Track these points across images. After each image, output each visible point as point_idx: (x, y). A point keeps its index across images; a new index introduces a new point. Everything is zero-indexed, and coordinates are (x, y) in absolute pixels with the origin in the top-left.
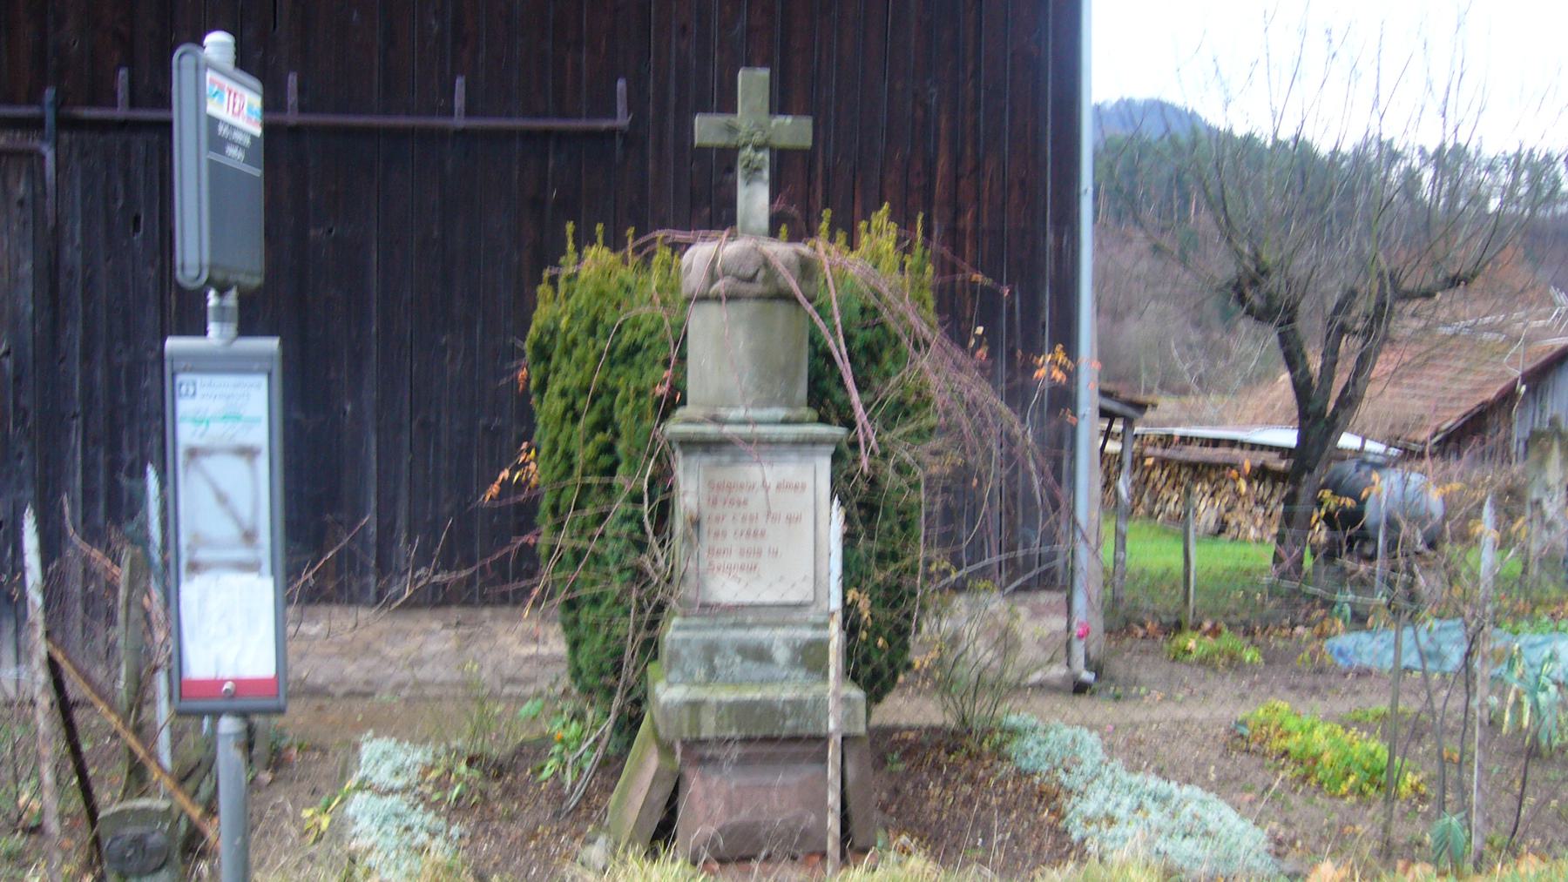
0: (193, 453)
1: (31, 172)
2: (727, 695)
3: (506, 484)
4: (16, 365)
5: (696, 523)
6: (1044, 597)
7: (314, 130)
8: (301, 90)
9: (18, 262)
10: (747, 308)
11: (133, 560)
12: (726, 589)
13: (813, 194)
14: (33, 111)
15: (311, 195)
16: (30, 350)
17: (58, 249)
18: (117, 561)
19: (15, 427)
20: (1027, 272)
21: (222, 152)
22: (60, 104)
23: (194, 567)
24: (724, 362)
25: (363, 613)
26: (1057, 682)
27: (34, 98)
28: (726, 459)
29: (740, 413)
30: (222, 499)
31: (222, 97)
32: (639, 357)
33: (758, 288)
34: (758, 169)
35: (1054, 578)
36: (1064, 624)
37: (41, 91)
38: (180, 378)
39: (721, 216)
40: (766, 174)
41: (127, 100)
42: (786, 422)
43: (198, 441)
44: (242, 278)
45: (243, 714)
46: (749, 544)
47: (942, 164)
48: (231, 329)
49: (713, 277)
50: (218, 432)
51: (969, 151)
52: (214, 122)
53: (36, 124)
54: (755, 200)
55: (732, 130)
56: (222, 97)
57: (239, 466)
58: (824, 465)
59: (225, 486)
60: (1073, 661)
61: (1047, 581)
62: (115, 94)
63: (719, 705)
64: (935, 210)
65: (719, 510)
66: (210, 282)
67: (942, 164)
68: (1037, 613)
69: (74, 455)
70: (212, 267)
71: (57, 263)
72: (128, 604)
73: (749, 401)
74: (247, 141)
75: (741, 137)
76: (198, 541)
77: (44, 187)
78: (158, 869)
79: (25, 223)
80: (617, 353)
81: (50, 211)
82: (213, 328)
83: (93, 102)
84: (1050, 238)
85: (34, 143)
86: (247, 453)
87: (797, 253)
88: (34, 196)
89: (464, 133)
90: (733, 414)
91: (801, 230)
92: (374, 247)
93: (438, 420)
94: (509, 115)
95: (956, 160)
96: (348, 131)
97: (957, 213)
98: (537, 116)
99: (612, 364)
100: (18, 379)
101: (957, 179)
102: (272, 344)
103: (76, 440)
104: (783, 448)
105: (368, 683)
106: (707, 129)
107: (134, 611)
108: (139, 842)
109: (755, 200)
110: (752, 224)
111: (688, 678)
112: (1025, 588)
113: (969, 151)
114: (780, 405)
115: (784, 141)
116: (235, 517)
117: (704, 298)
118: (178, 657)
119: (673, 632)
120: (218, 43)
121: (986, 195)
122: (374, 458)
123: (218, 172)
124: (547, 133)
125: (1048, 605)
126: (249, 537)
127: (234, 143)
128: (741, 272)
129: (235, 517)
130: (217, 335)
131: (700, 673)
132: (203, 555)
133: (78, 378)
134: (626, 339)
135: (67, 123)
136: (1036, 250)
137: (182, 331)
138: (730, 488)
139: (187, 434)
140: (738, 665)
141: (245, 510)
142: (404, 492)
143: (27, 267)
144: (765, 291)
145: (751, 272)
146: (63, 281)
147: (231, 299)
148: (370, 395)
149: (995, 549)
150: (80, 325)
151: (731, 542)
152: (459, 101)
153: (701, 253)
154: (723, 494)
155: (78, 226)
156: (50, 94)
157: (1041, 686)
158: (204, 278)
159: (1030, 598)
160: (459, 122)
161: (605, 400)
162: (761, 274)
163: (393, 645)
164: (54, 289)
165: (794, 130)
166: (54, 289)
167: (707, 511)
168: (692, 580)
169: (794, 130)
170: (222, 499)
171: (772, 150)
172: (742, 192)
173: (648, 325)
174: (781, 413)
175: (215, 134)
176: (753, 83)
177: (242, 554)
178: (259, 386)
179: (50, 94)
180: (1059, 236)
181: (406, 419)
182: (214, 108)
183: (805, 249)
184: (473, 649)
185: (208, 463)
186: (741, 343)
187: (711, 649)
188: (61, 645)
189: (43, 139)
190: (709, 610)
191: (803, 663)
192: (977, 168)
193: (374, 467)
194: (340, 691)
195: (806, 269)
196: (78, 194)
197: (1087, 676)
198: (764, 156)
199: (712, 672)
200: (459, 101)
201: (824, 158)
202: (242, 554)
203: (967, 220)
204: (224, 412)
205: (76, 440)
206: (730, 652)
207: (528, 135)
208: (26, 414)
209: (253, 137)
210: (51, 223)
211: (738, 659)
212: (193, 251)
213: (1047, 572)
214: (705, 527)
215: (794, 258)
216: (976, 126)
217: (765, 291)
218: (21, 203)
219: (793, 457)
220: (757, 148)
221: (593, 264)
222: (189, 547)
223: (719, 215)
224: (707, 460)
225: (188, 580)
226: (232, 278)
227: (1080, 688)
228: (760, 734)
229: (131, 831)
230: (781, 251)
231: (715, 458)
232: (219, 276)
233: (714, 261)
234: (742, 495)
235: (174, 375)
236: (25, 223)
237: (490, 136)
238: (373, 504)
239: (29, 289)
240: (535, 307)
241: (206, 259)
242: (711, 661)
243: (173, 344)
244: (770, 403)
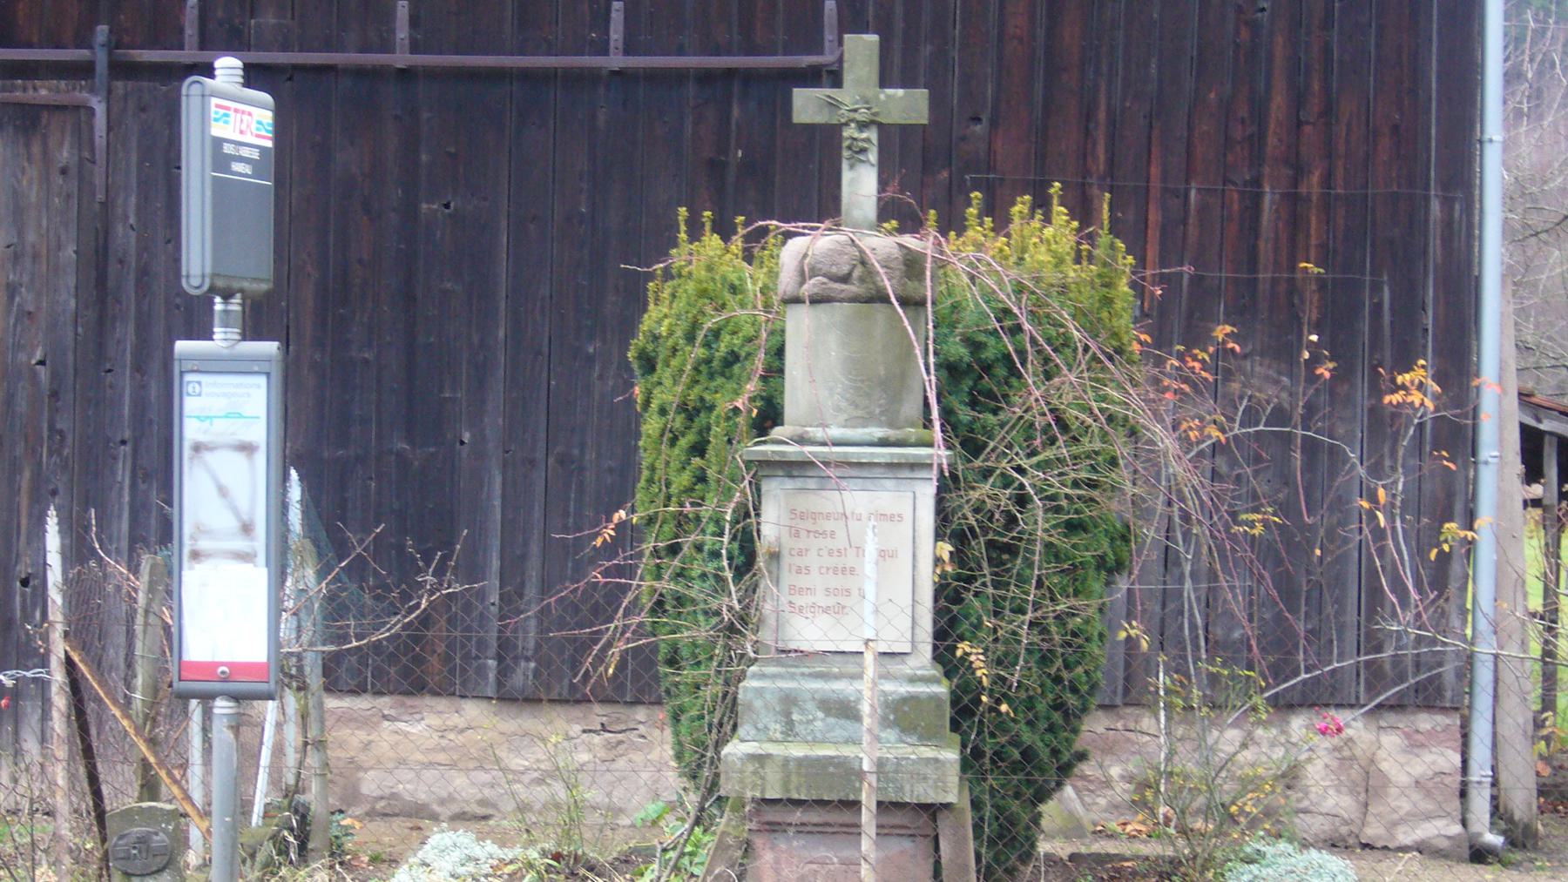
0: (198, 448)
1: (77, 131)
2: (797, 751)
3: (621, 526)
4: (54, 375)
5: (775, 556)
6: (1425, 722)
7: (433, 74)
8: (414, 22)
9: (59, 247)
10: (841, 311)
11: (153, 567)
12: (808, 633)
13: (928, 180)
14: (81, 54)
15: (424, 158)
16: (71, 357)
17: (107, 232)
18: (134, 569)
19: (50, 454)
20: (1404, 259)
21: (229, 171)
22: (115, 44)
23: (196, 555)
24: (819, 370)
25: (472, 710)
26: (1444, 844)
27: (83, 41)
28: (812, 483)
29: (835, 432)
30: (223, 491)
31: (232, 116)
32: (736, 368)
33: (853, 289)
34: (863, 151)
35: (1439, 691)
36: (1457, 759)
37: (91, 30)
38: (188, 377)
39: (822, 204)
40: (873, 156)
41: (196, 39)
42: (884, 443)
43: (202, 438)
44: (246, 285)
45: (237, 698)
46: (836, 582)
47: (1279, 103)
48: (234, 333)
49: (802, 278)
50: (220, 430)
51: (1316, 86)
52: (218, 142)
53: (83, 71)
54: (861, 185)
55: (834, 105)
56: (232, 116)
57: (239, 458)
58: (927, 492)
59: (226, 480)
60: (1471, 817)
61: (1428, 697)
62: (181, 31)
63: (786, 761)
64: (1266, 170)
65: (802, 543)
66: (213, 290)
67: (1279, 103)
68: (1415, 744)
69: (120, 495)
70: (214, 275)
71: (106, 248)
72: (147, 612)
73: (842, 417)
74: (255, 155)
75: (843, 114)
76: (201, 531)
77: (93, 151)
78: (159, 871)
79: (69, 196)
80: (715, 364)
81: (99, 181)
82: (218, 332)
83: (154, 43)
84: (1435, 207)
85: (82, 96)
86: (247, 448)
87: (901, 246)
88: (81, 159)
89: (619, 73)
90: (819, 433)
91: (910, 223)
92: (504, 223)
93: (582, 453)
94: (681, 52)
95: (1298, 100)
96: (473, 74)
97: (1299, 171)
98: (717, 52)
99: (711, 376)
100: (54, 395)
101: (1300, 124)
102: (271, 347)
103: (123, 473)
104: (877, 472)
105: (483, 802)
106: (807, 105)
107: (152, 619)
108: (143, 841)
109: (861, 185)
110: (857, 214)
111: (763, 733)
112: (1397, 706)
113: (1316, 86)
114: (880, 425)
115: (894, 117)
116: (235, 511)
117: (796, 300)
118: (171, 636)
119: (755, 686)
120: (228, 67)
121: (1342, 149)
122: (497, 503)
123: (221, 190)
124: (730, 73)
125: (1431, 734)
126: (247, 529)
127: (241, 159)
128: (834, 270)
129: (235, 511)
130: (223, 339)
131: (776, 729)
132: (204, 544)
133: (127, 392)
134: (723, 348)
135: (122, 70)
136: (1415, 222)
137: (189, 337)
138: (815, 516)
139: (192, 429)
140: (820, 722)
141: (243, 504)
142: (535, 549)
143: (70, 252)
144: (855, 289)
145: (845, 269)
146: (113, 268)
147: (235, 305)
148: (494, 422)
149: (1351, 645)
150: (131, 328)
151: (815, 580)
152: (616, 34)
153: (802, 249)
154: (809, 525)
155: (133, 200)
156: (102, 32)
157: (1421, 848)
158: (206, 287)
159: (1402, 721)
160: (616, 61)
161: (702, 419)
162: (856, 274)
163: (517, 751)
164: (101, 281)
165: (907, 105)
166: (101, 281)
167: (788, 543)
168: (771, 621)
169: (907, 105)
170: (223, 491)
171: (883, 128)
172: (847, 175)
173: (748, 330)
174: (878, 432)
175: (220, 156)
176: (861, 50)
177: (241, 544)
178: (259, 386)
179: (102, 32)
180: (1447, 203)
181: (540, 455)
182: (217, 130)
183: (910, 241)
184: (621, 763)
185: (208, 457)
186: (833, 350)
187: (789, 702)
188: (84, 647)
189: (92, 91)
190: (789, 655)
191: (895, 724)
192: (1328, 110)
193: (499, 517)
194: (445, 812)
195: (912, 264)
196: (134, 159)
197: (1494, 839)
198: (872, 134)
199: (790, 726)
200: (616, 34)
201: (1109, 98)
202: (241, 544)
203: (1313, 184)
204: (228, 409)
205: (123, 473)
206: (810, 706)
207: (706, 77)
208: (63, 438)
209: (262, 149)
210: (100, 197)
211: (820, 715)
212: (197, 263)
213: (1430, 680)
214: (786, 560)
215: (896, 253)
216: (1327, 50)
217: (855, 289)
218: (64, 171)
219: (889, 483)
220: (863, 126)
221: (704, 256)
222: (192, 537)
223: (822, 204)
224: (789, 484)
225: (191, 568)
226: (235, 285)
227: (1480, 855)
228: (834, 797)
229: (137, 830)
230: (882, 245)
231: (799, 483)
232: (220, 283)
233: (805, 256)
234: (829, 526)
235: (182, 373)
236: (69, 196)
237: (653, 77)
238: (495, 564)
239: (72, 281)
240: (645, 310)
241: (208, 270)
242: (788, 714)
243: (181, 346)
244: (865, 422)
